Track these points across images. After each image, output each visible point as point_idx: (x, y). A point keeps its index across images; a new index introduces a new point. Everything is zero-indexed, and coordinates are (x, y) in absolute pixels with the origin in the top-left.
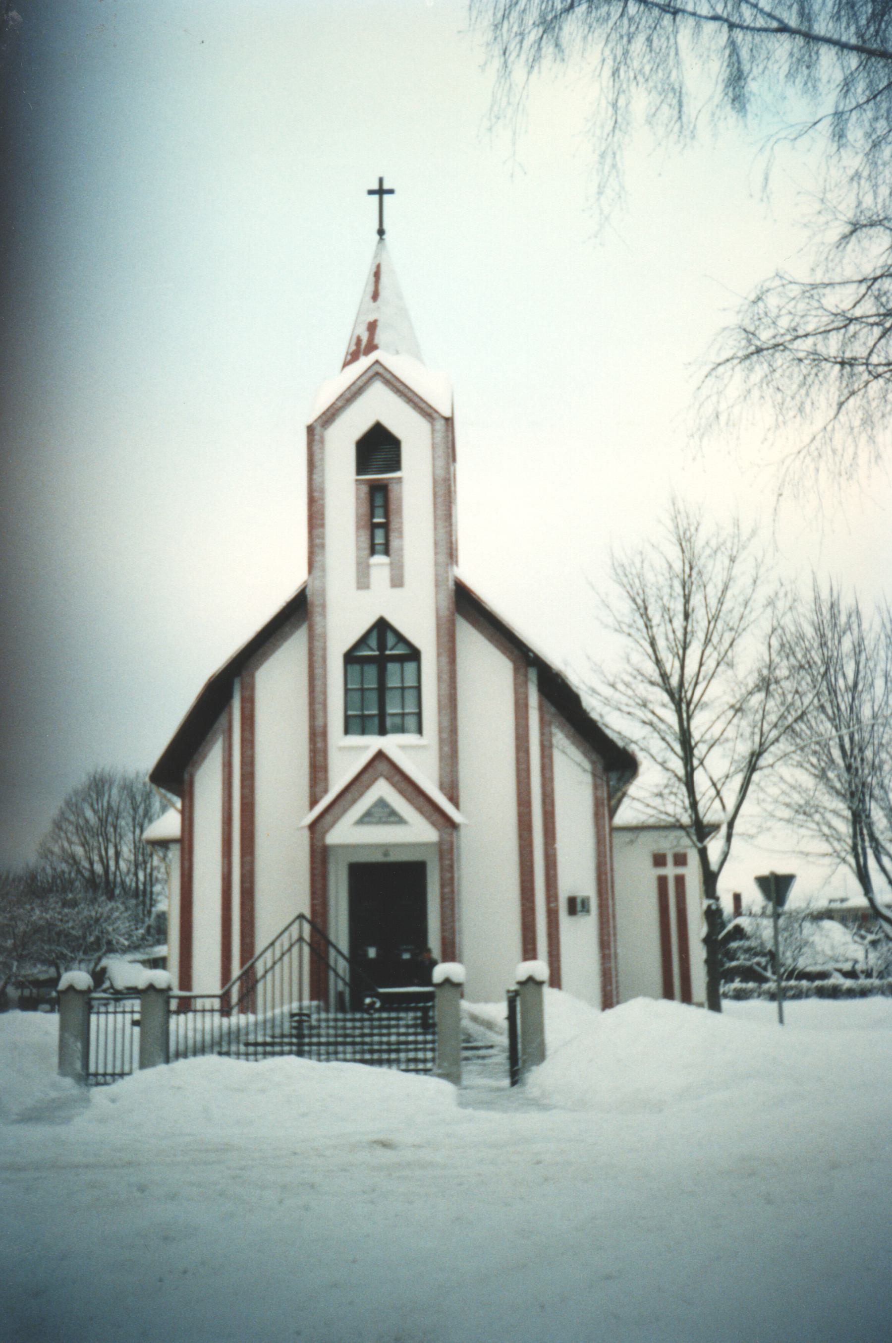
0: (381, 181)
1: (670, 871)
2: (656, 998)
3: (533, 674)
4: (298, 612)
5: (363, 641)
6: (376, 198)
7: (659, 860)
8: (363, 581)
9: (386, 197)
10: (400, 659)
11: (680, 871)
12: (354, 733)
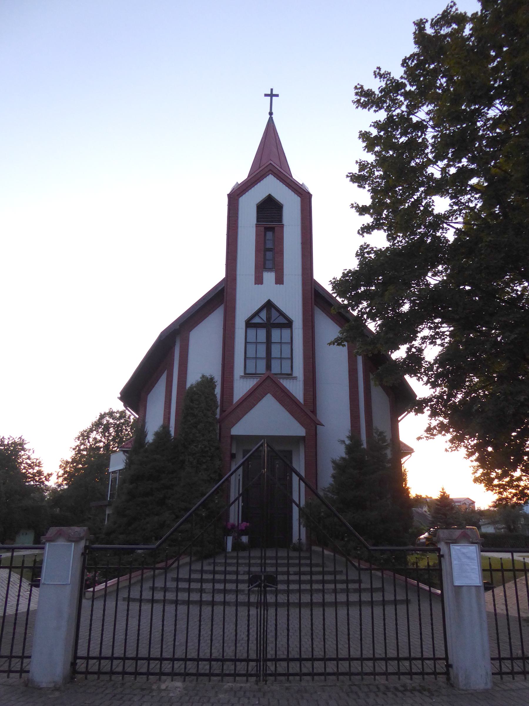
0: (272, 90)
5: (257, 313)
6: (269, 98)
8: (259, 280)
9: (274, 98)
10: (281, 326)
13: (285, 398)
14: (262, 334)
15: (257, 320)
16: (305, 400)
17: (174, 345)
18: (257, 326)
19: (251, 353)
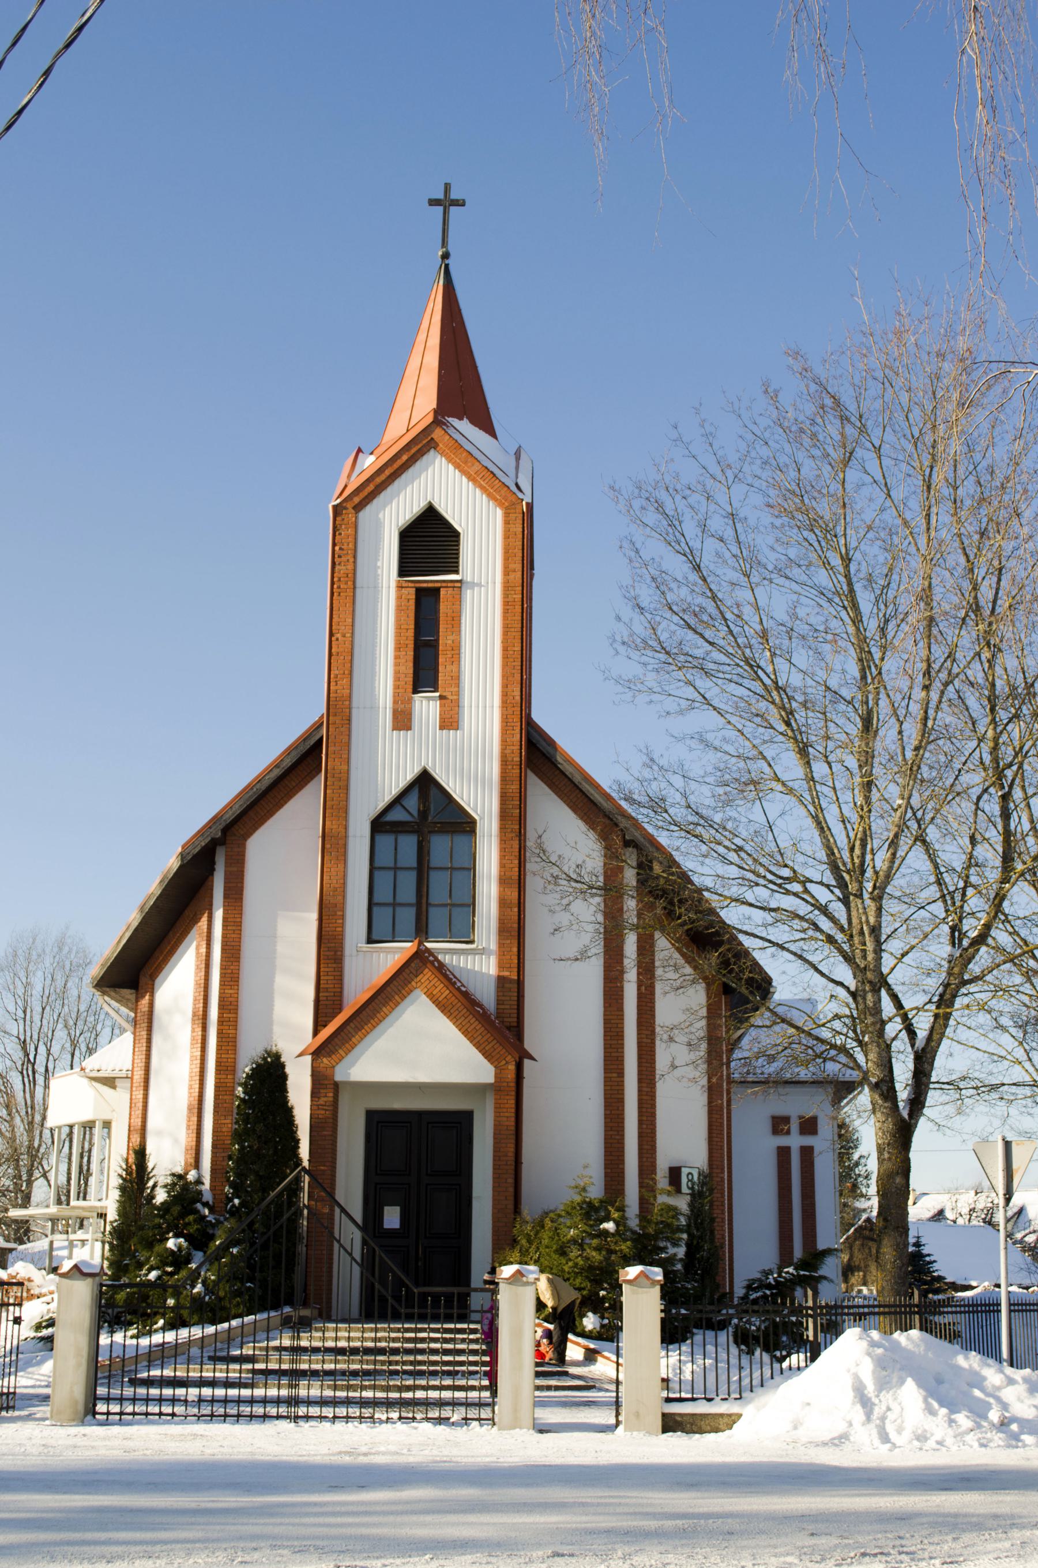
0: (447, 187)
1: (795, 1141)
2: (649, 1433)
3: (631, 857)
4: (306, 762)
5: (397, 801)
7: (779, 1124)
8: (403, 720)
11: (808, 1141)
12: (458, 567)
13: (459, 1002)
14: (408, 844)
15: (397, 815)
16: (499, 1002)
17: (211, 870)
18: (397, 828)
19: (384, 895)
